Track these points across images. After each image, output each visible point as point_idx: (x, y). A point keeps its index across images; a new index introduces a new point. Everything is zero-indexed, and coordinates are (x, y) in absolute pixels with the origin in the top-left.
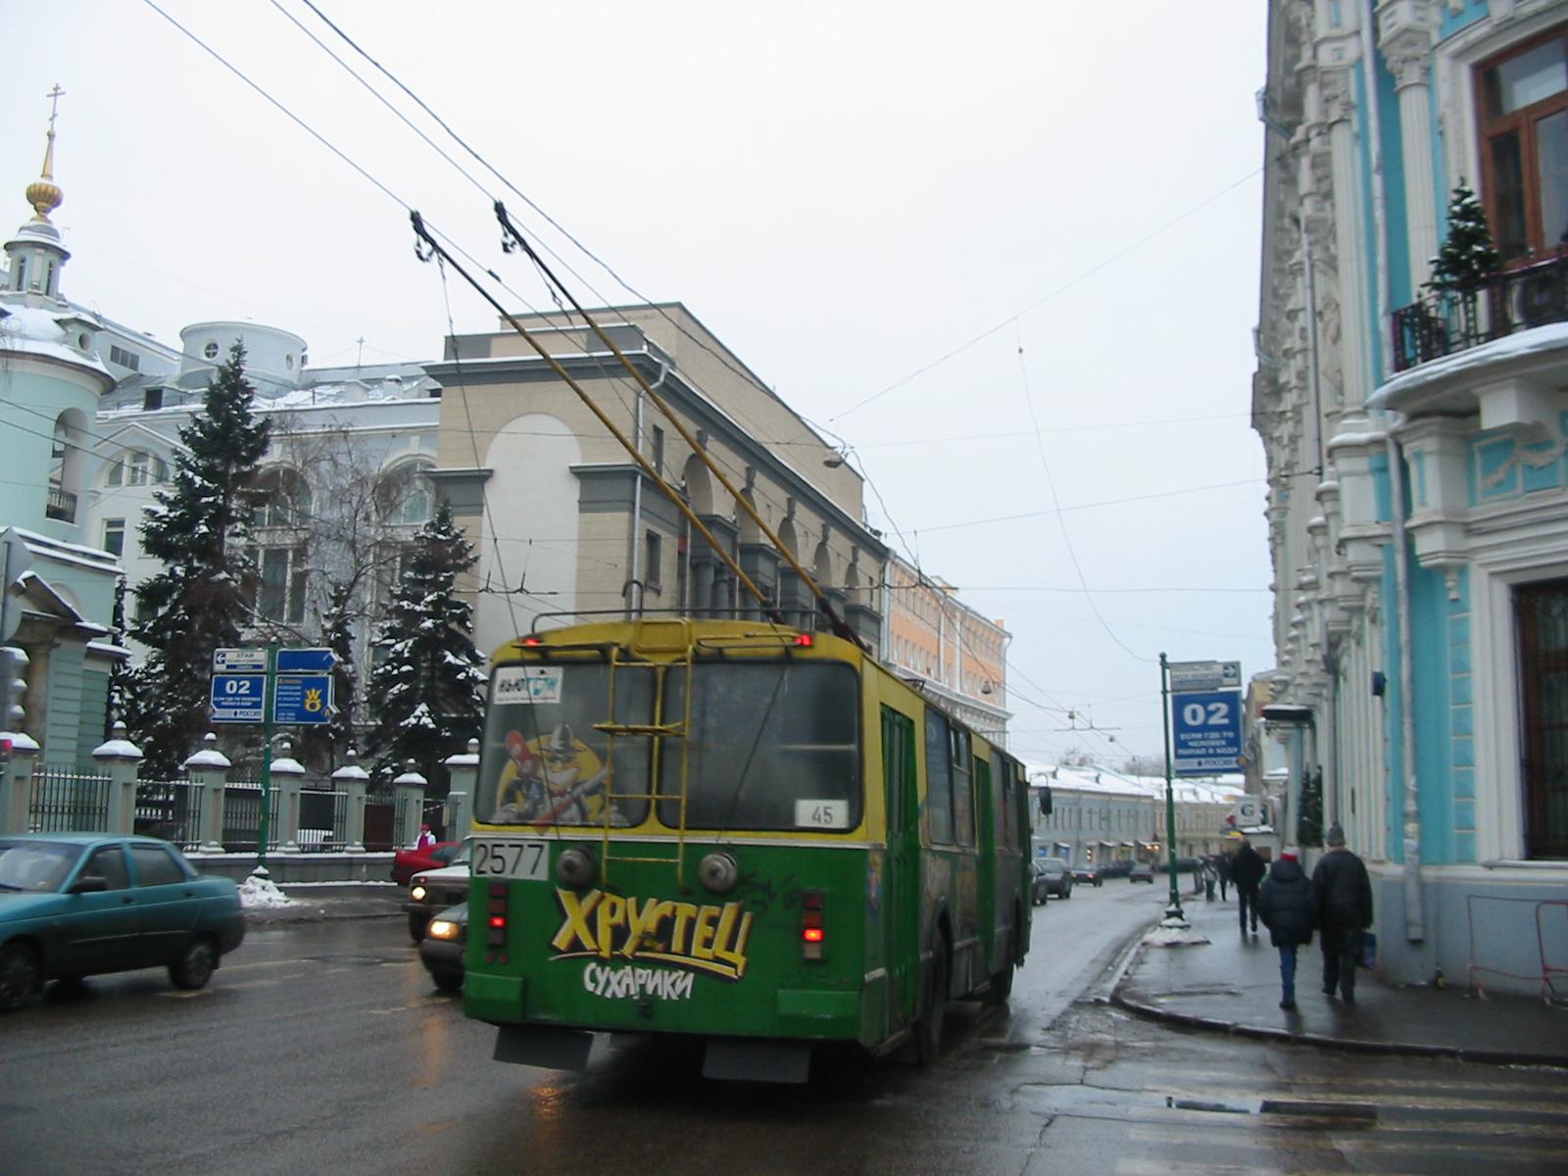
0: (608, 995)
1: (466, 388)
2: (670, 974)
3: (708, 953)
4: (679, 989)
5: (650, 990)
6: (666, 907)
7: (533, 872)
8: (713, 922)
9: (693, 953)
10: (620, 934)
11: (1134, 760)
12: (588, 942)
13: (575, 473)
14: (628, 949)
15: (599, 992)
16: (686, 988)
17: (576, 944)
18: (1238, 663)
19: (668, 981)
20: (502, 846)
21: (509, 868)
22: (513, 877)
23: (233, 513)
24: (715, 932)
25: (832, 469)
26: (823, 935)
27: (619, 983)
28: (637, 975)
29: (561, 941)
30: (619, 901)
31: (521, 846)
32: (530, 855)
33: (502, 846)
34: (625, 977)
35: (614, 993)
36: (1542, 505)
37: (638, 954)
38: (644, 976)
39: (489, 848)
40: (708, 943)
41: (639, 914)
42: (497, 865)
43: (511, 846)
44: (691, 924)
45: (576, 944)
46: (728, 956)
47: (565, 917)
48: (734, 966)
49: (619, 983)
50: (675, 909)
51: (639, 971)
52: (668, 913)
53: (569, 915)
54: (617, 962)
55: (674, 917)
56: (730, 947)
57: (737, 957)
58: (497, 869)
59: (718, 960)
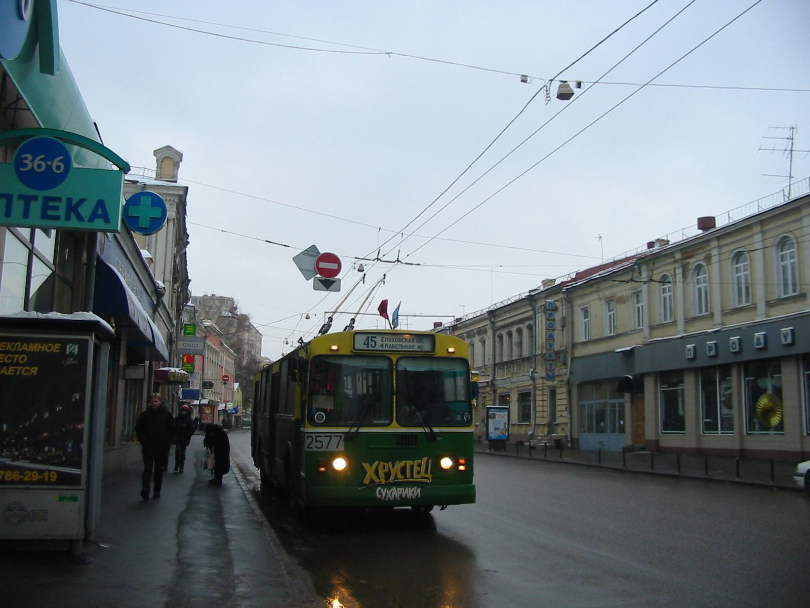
0: (387, 499)
1: (47, 277)
2: (411, 489)
3: (419, 476)
4: (415, 494)
5: (404, 496)
6: (403, 463)
7: (337, 447)
8: (419, 465)
9: (414, 477)
10: (387, 475)
12: (377, 481)
13: (319, 280)
14: (391, 480)
15: (383, 499)
16: (418, 493)
17: (372, 481)
18: (435, 323)
19: (411, 492)
20: (321, 436)
21: (325, 445)
22: (327, 450)
23: (72, 427)
24: (421, 468)
25: (170, 145)
26: (458, 468)
27: (391, 495)
28: (398, 491)
29: (367, 481)
30: (386, 464)
31: (331, 437)
32: (335, 440)
33: (321, 436)
34: (393, 492)
35: (389, 499)
36: (517, 314)
37: (395, 481)
38: (401, 491)
39: (314, 438)
40: (419, 473)
41: (393, 467)
42: (319, 445)
43: (325, 436)
44: (412, 467)
45: (372, 481)
46: (426, 476)
47: (366, 472)
48: (428, 478)
49: (391, 495)
50: (406, 463)
51: (399, 489)
52: (404, 465)
53: (367, 471)
54: (389, 485)
55: (406, 466)
56: (426, 472)
57: (429, 475)
58: (318, 447)
59: (423, 478)
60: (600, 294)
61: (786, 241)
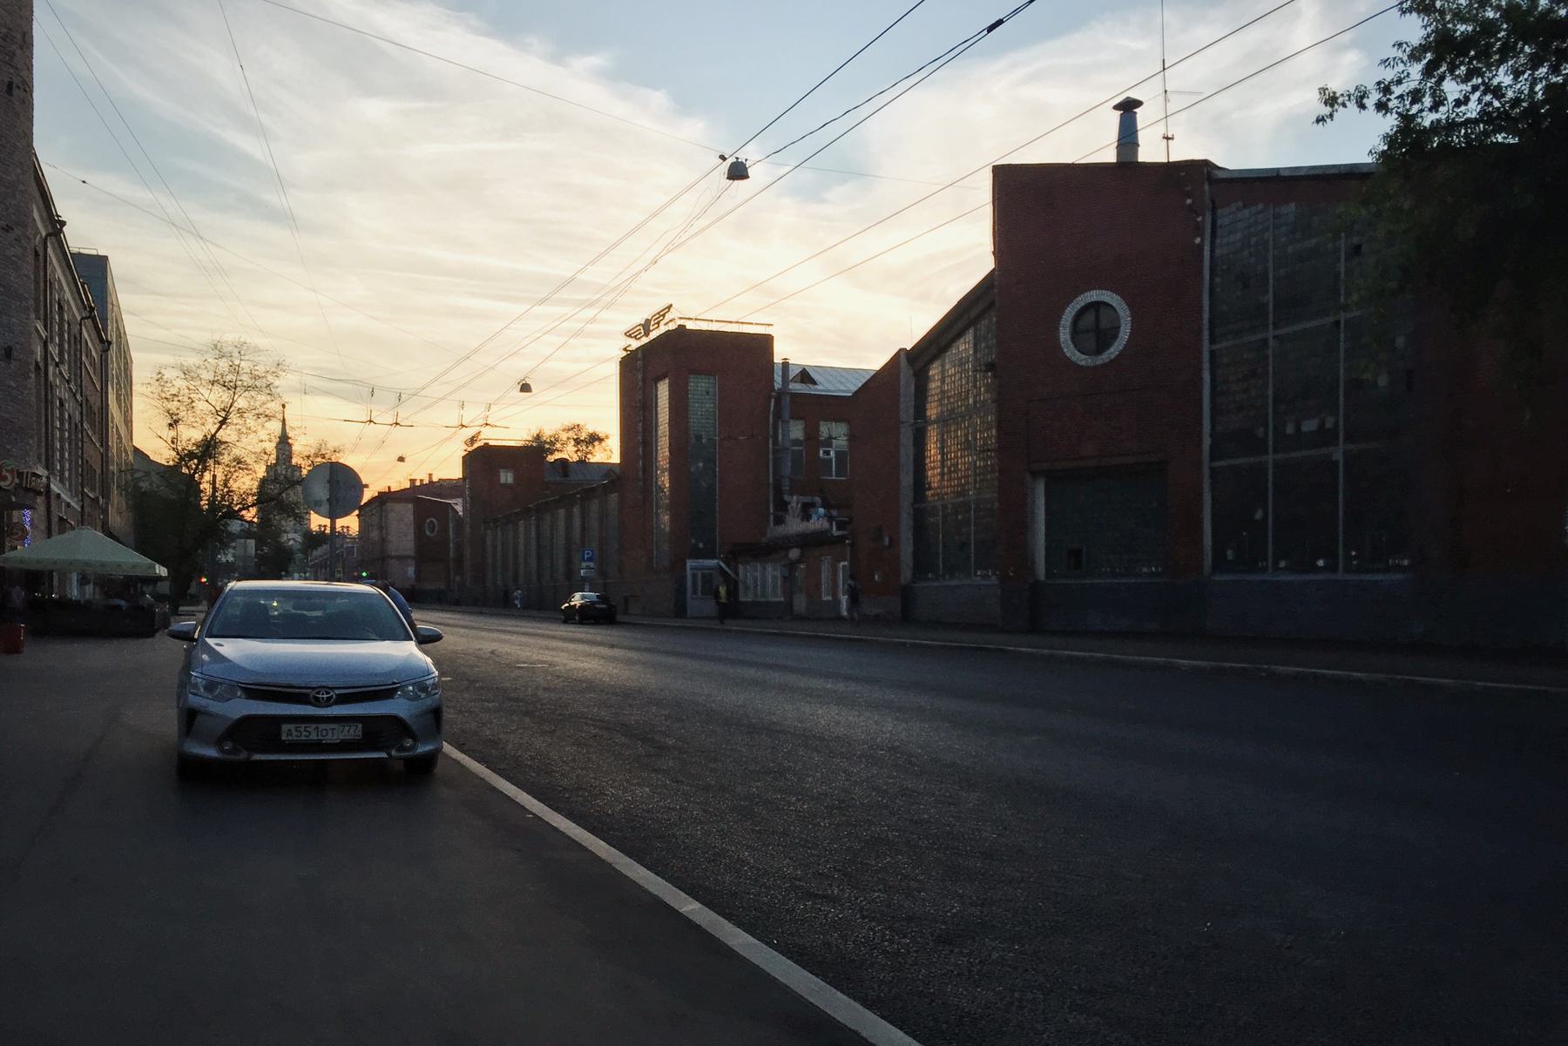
18: (102, 261)
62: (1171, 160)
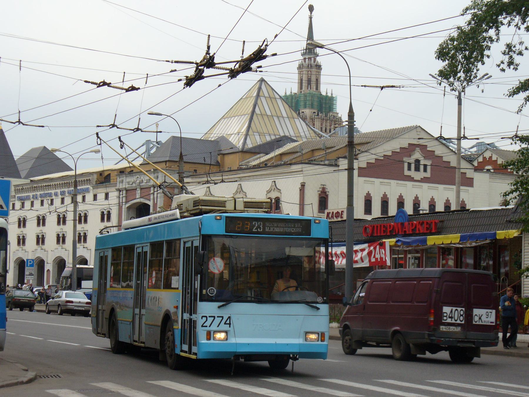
11: (355, 121)
18: (473, 179)
60: (218, 272)
61: (109, 349)
62: (297, 72)
